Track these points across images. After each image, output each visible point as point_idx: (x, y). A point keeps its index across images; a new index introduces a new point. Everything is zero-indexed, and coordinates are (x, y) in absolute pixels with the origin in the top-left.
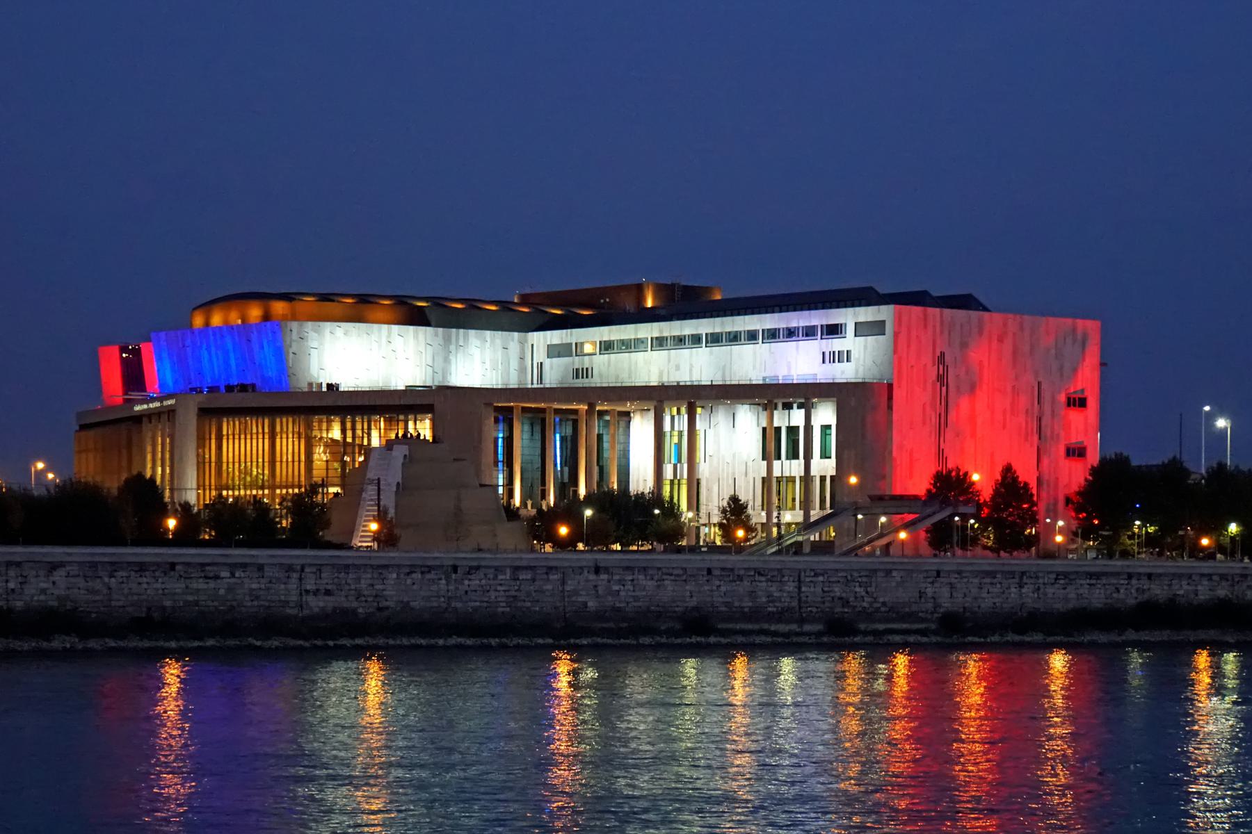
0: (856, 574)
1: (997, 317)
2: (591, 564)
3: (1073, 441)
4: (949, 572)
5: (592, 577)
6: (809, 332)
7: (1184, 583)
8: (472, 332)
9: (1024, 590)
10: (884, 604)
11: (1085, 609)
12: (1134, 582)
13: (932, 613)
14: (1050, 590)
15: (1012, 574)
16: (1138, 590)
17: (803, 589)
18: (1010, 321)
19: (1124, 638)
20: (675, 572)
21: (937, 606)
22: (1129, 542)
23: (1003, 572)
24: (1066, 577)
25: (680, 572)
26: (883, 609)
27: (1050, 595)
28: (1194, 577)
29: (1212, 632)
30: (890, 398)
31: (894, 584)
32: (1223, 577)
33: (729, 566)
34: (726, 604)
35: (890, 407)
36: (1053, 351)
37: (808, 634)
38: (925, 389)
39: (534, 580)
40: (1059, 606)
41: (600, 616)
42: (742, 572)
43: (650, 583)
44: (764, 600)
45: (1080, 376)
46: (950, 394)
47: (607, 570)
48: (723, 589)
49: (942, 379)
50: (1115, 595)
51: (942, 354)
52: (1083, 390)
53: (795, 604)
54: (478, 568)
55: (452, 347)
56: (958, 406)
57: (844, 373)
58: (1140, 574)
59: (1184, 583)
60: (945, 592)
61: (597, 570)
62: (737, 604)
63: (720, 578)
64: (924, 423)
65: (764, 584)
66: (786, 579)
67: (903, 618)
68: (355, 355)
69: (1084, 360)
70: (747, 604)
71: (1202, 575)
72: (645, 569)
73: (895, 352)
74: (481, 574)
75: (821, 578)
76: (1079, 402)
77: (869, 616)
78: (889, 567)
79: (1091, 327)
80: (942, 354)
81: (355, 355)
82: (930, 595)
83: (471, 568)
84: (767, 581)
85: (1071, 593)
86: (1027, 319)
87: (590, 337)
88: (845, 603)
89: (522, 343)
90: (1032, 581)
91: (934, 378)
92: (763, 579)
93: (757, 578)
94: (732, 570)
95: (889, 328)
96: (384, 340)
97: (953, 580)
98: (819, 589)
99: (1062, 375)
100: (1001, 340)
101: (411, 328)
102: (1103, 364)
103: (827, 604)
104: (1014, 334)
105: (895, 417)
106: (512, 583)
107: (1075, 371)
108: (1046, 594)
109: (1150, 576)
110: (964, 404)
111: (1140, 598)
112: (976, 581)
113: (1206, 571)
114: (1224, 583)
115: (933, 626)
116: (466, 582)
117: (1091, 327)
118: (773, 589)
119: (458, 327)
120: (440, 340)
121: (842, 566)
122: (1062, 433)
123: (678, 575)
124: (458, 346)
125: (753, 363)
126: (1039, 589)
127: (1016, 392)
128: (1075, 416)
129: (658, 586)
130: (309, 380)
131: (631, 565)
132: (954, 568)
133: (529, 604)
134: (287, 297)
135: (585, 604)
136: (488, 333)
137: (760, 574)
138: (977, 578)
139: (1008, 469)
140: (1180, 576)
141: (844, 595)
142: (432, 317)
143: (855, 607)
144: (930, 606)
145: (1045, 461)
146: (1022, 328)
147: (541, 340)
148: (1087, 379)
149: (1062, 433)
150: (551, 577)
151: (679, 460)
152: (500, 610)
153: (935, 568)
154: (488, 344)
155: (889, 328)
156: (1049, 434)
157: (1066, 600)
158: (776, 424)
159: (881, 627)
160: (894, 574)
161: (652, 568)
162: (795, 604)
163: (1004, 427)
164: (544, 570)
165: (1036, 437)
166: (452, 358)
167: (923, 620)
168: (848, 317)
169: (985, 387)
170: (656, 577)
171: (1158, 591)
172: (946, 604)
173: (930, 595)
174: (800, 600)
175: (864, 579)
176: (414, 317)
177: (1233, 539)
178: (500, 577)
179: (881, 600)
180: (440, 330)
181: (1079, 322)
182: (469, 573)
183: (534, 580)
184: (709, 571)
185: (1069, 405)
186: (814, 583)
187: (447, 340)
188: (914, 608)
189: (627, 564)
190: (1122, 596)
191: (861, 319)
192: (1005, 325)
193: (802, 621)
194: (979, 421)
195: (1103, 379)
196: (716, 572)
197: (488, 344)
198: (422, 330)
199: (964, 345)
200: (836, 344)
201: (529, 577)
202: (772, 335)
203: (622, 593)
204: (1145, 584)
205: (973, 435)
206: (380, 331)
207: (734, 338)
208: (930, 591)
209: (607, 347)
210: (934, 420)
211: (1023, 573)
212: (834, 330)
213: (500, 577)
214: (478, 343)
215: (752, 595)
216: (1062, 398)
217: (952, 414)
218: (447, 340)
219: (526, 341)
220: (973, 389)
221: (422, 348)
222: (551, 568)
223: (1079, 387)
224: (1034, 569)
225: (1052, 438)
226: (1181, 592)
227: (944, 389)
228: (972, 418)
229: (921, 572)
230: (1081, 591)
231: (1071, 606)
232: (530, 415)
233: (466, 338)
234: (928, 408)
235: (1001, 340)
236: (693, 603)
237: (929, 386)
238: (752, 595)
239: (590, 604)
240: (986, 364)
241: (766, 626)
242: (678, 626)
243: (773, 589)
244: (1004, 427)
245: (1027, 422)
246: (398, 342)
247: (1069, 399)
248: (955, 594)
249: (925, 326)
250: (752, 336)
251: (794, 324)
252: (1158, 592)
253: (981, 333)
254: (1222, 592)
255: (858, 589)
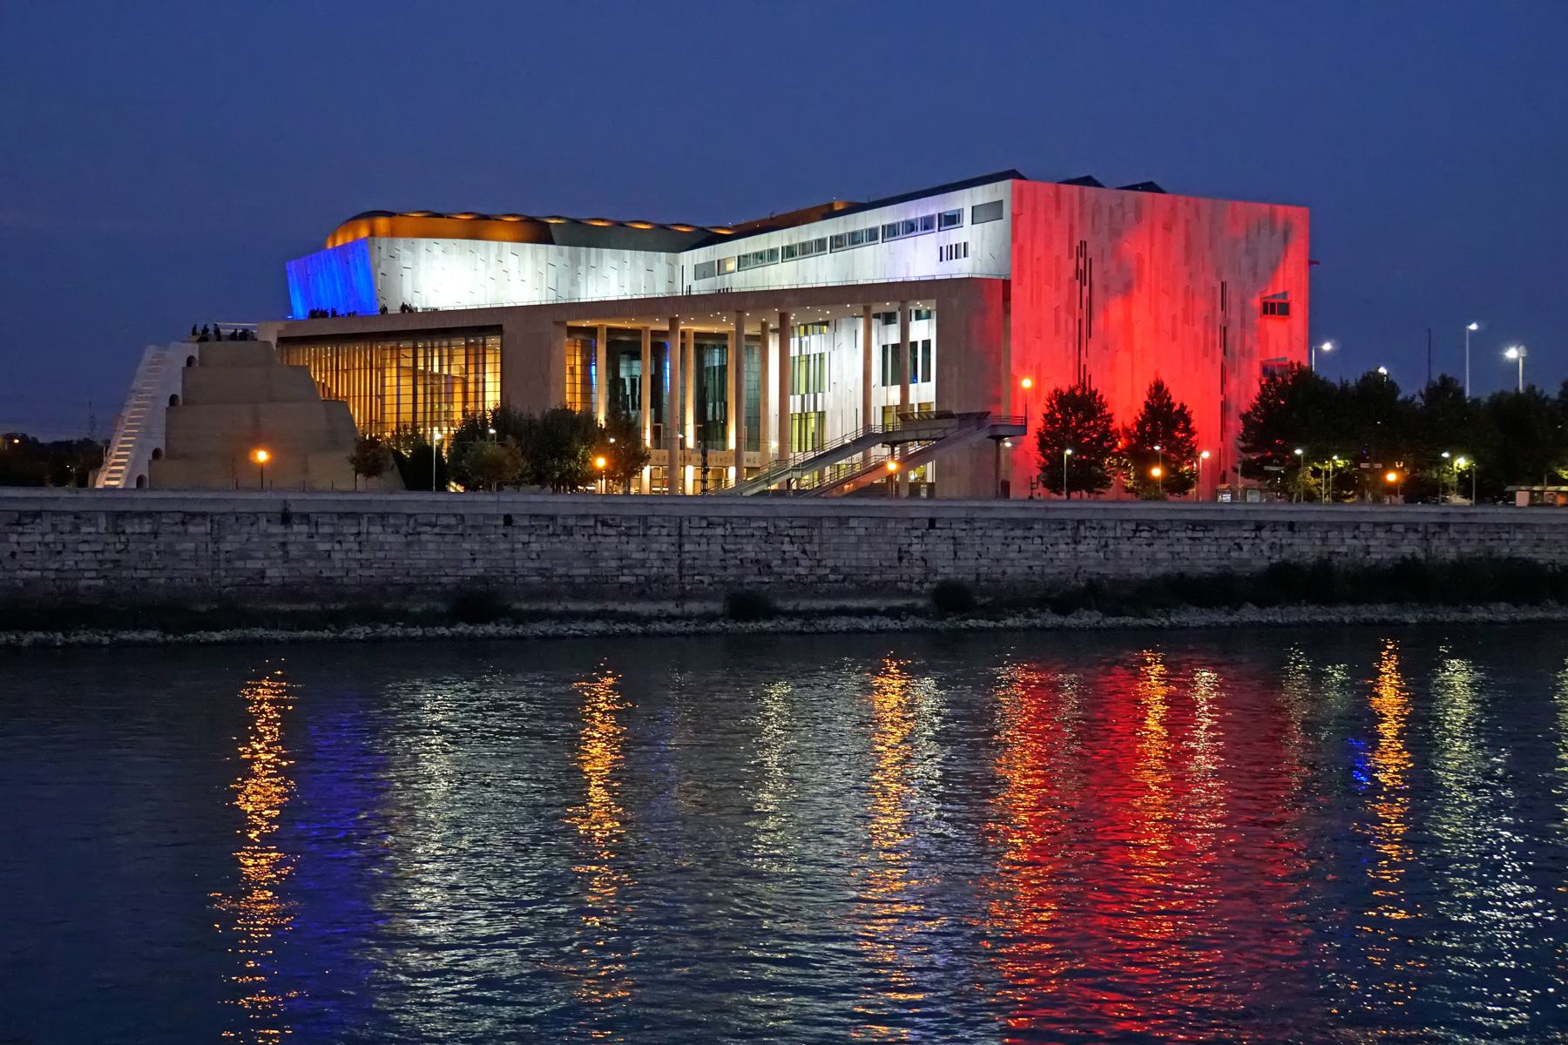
0: (783, 524)
1: (1170, 197)
2: (278, 508)
3: (1273, 356)
4: (950, 521)
5: (277, 529)
6: (927, 224)
7: (1347, 535)
8: (606, 251)
9: (1081, 548)
10: (835, 569)
11: (1182, 575)
12: (1265, 534)
13: (920, 583)
14: (1126, 547)
15: (1061, 524)
16: (1272, 546)
17: (687, 547)
18: (1181, 205)
19: (1235, 618)
20: (443, 521)
21: (929, 570)
22: (1313, 481)
23: (1044, 520)
24: (1151, 529)
25: (453, 521)
26: (832, 577)
27: (1125, 555)
28: (1363, 528)
29: (1383, 608)
30: (1007, 298)
31: (853, 540)
32: (1411, 527)
33: (549, 511)
34: (541, 572)
35: (1007, 311)
36: (1243, 245)
37: (689, 617)
38: (1057, 289)
39: (156, 534)
40: (1140, 570)
41: (288, 591)
42: (571, 522)
43: (390, 538)
44: (613, 564)
45: (1280, 276)
46: (1095, 298)
47: (305, 518)
48: (535, 547)
49: (1082, 276)
50: (1234, 554)
51: (1083, 244)
52: (1285, 294)
53: (672, 570)
54: (37, 515)
55: (582, 269)
56: (1106, 311)
57: (961, 268)
58: (1276, 523)
59: (1347, 535)
60: (946, 548)
61: (286, 518)
62: (561, 571)
63: (530, 530)
64: (1057, 332)
65: (615, 540)
66: (655, 531)
67: (866, 590)
68: (447, 275)
69: (1286, 256)
70: (581, 571)
71: (1376, 524)
72: (383, 516)
73: (1014, 238)
74: (45, 524)
75: (720, 531)
76: (1275, 308)
77: (802, 587)
78: (844, 513)
79: (1298, 215)
80: (1083, 244)
81: (447, 275)
82: (917, 555)
83: (23, 514)
84: (620, 535)
85: (1161, 551)
86: (1206, 205)
87: (730, 251)
88: (763, 566)
89: (671, 265)
90: (1095, 533)
91: (1071, 272)
92: (613, 532)
93: (599, 529)
94: (552, 518)
95: (1007, 211)
96: (493, 259)
97: (959, 533)
98: (716, 548)
99: (1255, 275)
100: (1168, 227)
101: (528, 246)
102: (1311, 263)
103: (733, 571)
104: (1187, 222)
105: (1014, 322)
106: (111, 539)
107: (1274, 269)
108: (1117, 553)
109: (1291, 526)
110: (1116, 311)
111: (1276, 558)
112: (999, 533)
113: (1381, 519)
114: (1411, 535)
115: (921, 603)
116: (14, 538)
117: (1298, 215)
118: (632, 548)
119: (588, 246)
120: (565, 259)
121: (759, 512)
122: (1257, 348)
123: (448, 526)
124: (589, 267)
125: (873, 264)
126: (1106, 545)
127: (1189, 294)
128: (1273, 326)
129: (409, 544)
130: (382, 303)
131: (359, 509)
132: (963, 514)
133: (145, 574)
134: (389, 214)
135: (262, 574)
136: (627, 252)
137: (604, 524)
138: (1115, 536)
139: (1158, 389)
140: (1340, 526)
141: (762, 556)
142: (555, 235)
143: (780, 575)
144: (918, 571)
145: (1233, 382)
146: (1197, 214)
147: (691, 259)
148: (1291, 280)
149: (1257, 348)
150: (192, 529)
151: (807, 391)
152: (83, 583)
153: (929, 515)
154: (628, 266)
155: (1007, 211)
156: (1238, 346)
157: (1154, 561)
158: (912, 339)
159: (820, 604)
160: (853, 523)
161: (396, 514)
162: (672, 570)
163: (1174, 338)
164: (178, 518)
165: (1219, 351)
166: (581, 279)
167: (909, 593)
168: (963, 201)
169: (1145, 288)
170: (404, 530)
171: (1306, 549)
172: (946, 569)
173: (917, 555)
174: (681, 566)
175: (799, 532)
176: (539, 233)
177: (1461, 475)
178: (84, 529)
179: (830, 563)
180: (566, 249)
181: (1280, 209)
182: (18, 523)
183: (156, 534)
184: (508, 520)
185: (1265, 312)
186: (708, 538)
187: (575, 261)
188: (891, 576)
189: (349, 508)
190: (1245, 555)
191: (979, 202)
192: (1173, 209)
193: (683, 597)
194: (1137, 331)
195: (1312, 280)
196: (518, 521)
197: (628, 266)
198: (541, 248)
199: (1115, 233)
200: (954, 236)
201: (147, 528)
202: (891, 232)
203: (337, 556)
204: (1283, 535)
205: (1129, 347)
206: (487, 248)
207: (855, 239)
208: (916, 549)
209: (743, 261)
210: (1072, 326)
211: (1080, 522)
212: (951, 220)
213: (84, 529)
214: (615, 264)
215: (590, 556)
216: (1256, 303)
217: (1098, 322)
218: (575, 261)
219: (676, 262)
220: (1127, 289)
221: (542, 268)
222: (193, 515)
223: (1281, 291)
224: (1100, 516)
225: (1242, 354)
226: (1343, 549)
227: (1086, 289)
228: (1127, 324)
229: (903, 520)
230: (1178, 548)
231: (1160, 570)
232: (582, 337)
233: (599, 258)
234: (1063, 315)
235: (1168, 227)
236: (478, 569)
237: (1065, 289)
238: (590, 556)
239: (269, 573)
240: (1147, 259)
241: (611, 606)
242: (442, 607)
243: (632, 548)
244: (1174, 338)
245: (1206, 333)
246: (511, 262)
247: (1265, 304)
248: (961, 554)
249: (1058, 207)
250: (872, 235)
251: (912, 217)
252: (1306, 549)
253: (1138, 219)
254: (1409, 548)
255: (786, 547)
